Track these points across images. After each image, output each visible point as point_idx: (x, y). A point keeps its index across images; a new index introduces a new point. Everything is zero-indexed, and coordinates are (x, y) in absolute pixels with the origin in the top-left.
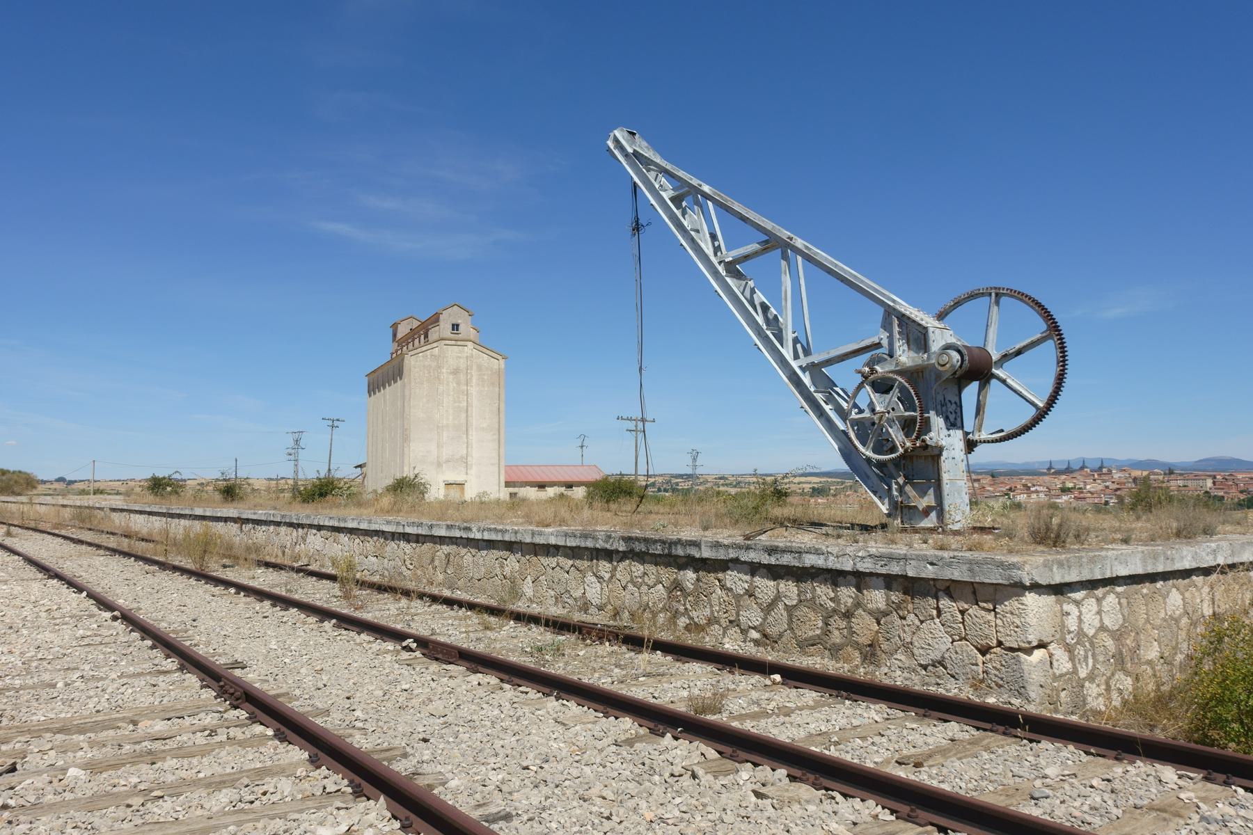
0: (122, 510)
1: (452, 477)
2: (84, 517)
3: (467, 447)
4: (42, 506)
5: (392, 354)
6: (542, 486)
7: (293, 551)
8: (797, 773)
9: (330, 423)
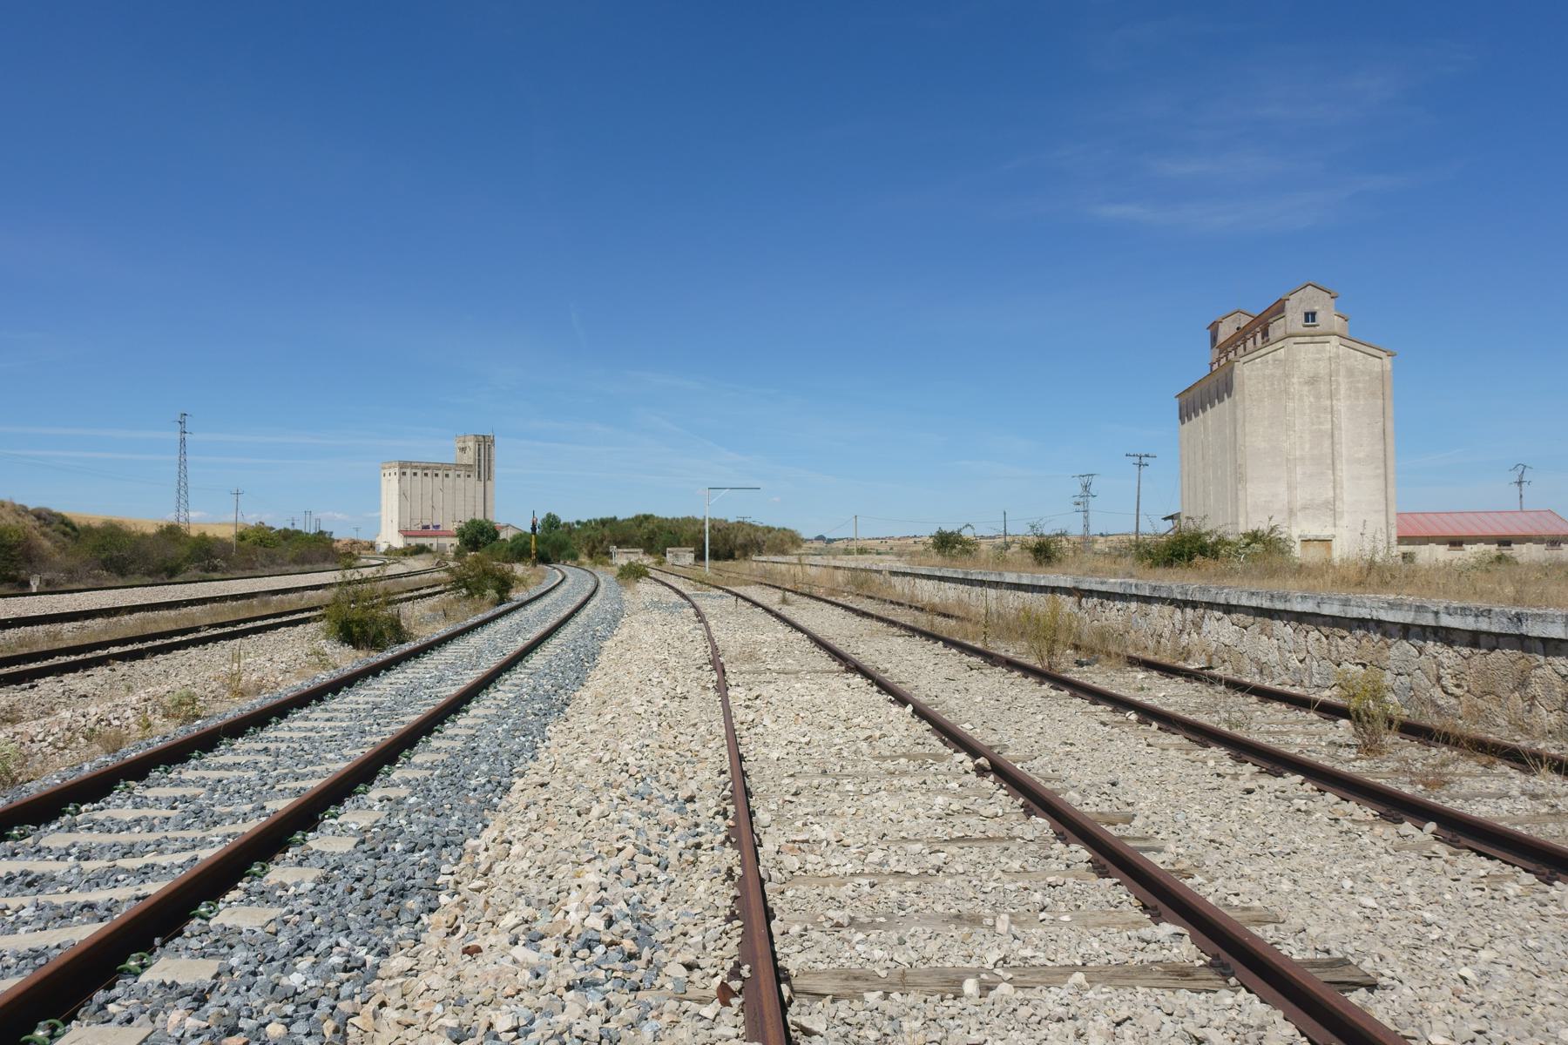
0: (905, 574)
1: (1314, 531)
2: (861, 582)
3: (1334, 488)
4: (814, 569)
5: (1212, 365)
6: (1456, 542)
7: (1177, 643)
8: (1163, 726)
9: (1136, 460)
